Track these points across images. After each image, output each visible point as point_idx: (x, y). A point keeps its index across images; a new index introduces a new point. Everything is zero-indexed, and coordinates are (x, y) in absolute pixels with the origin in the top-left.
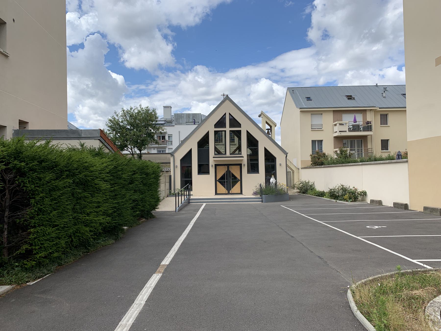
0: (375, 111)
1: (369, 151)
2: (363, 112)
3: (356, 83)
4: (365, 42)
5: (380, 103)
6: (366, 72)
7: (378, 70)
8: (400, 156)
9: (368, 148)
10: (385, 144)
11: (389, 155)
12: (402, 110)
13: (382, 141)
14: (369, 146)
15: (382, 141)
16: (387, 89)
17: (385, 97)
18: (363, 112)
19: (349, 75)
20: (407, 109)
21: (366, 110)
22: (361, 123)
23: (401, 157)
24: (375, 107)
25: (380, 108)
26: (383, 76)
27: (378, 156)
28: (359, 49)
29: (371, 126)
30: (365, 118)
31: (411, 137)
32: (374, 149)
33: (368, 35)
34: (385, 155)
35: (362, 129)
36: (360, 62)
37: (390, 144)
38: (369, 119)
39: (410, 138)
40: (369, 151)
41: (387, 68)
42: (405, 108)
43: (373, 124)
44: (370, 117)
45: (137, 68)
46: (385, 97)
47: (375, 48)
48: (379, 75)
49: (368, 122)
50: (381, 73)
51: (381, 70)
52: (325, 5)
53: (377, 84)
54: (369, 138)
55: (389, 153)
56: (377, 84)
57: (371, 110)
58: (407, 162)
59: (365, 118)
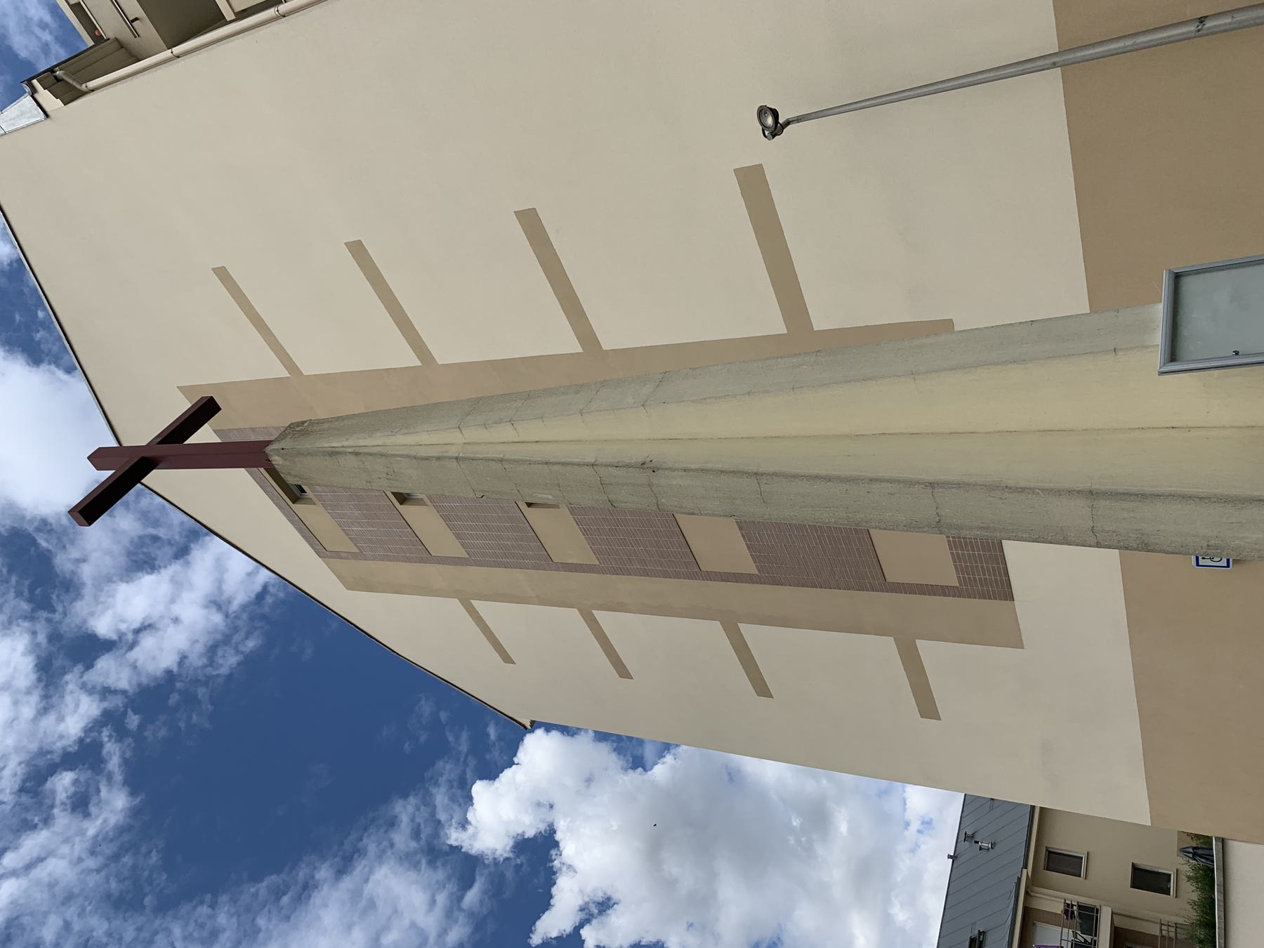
0: (1033, 882)
1: (1172, 935)
2: (1030, 917)
3: (935, 905)
4: (820, 850)
5: (1011, 864)
6: (904, 864)
7: (906, 833)
8: (1200, 852)
9: (1158, 933)
10: (1145, 879)
11: (1189, 878)
12: (1041, 818)
13: (1136, 883)
14: (1154, 930)
15: (1136, 883)
16: (969, 833)
17: (993, 845)
18: (1030, 917)
19: (900, 915)
20: (1038, 804)
21: (1026, 909)
22: (1068, 934)
23: (1206, 857)
24: (1019, 879)
25: (1025, 866)
26: (927, 824)
27: (1192, 915)
28: (834, 865)
29: (1080, 907)
30: (1051, 919)
31: (1133, 806)
32: (1166, 918)
33: (803, 839)
34: (1190, 892)
35: (1089, 938)
36: (871, 873)
37: (1147, 863)
38: (1059, 908)
39: (1143, 817)
40: (1172, 935)
41: (905, 810)
42: (1033, 807)
43: (1075, 899)
44: (1052, 903)
45: (554, 890)
46: (993, 845)
47: (843, 828)
48: (919, 831)
49: (1066, 912)
50: (916, 825)
51: (907, 824)
52: (691, 925)
53: (950, 857)
54: (1121, 923)
55: (1183, 878)
56: (950, 857)
57: (1027, 893)
58: (1223, 841)
59: (1051, 919)
